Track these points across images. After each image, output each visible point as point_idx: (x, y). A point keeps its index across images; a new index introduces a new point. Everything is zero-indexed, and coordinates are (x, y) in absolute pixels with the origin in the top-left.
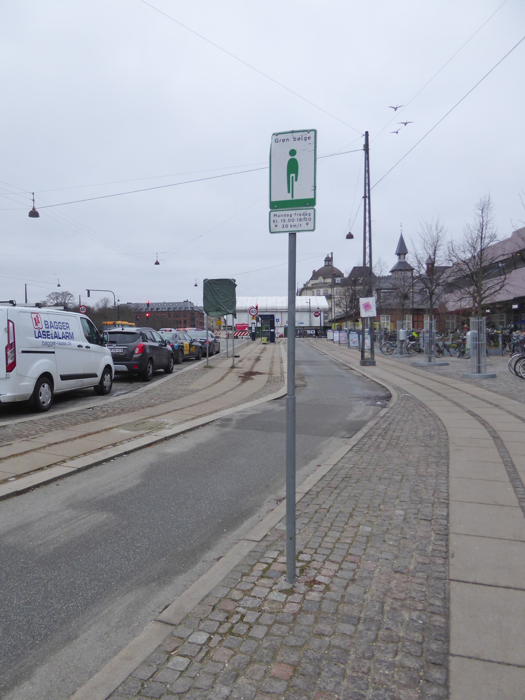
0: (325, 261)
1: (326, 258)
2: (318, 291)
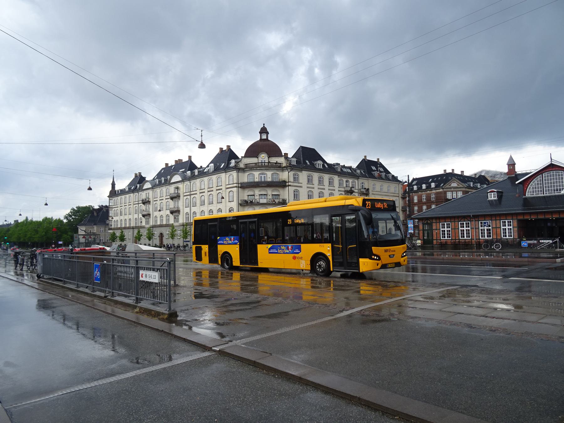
0: (261, 133)
1: (262, 129)
2: (263, 174)
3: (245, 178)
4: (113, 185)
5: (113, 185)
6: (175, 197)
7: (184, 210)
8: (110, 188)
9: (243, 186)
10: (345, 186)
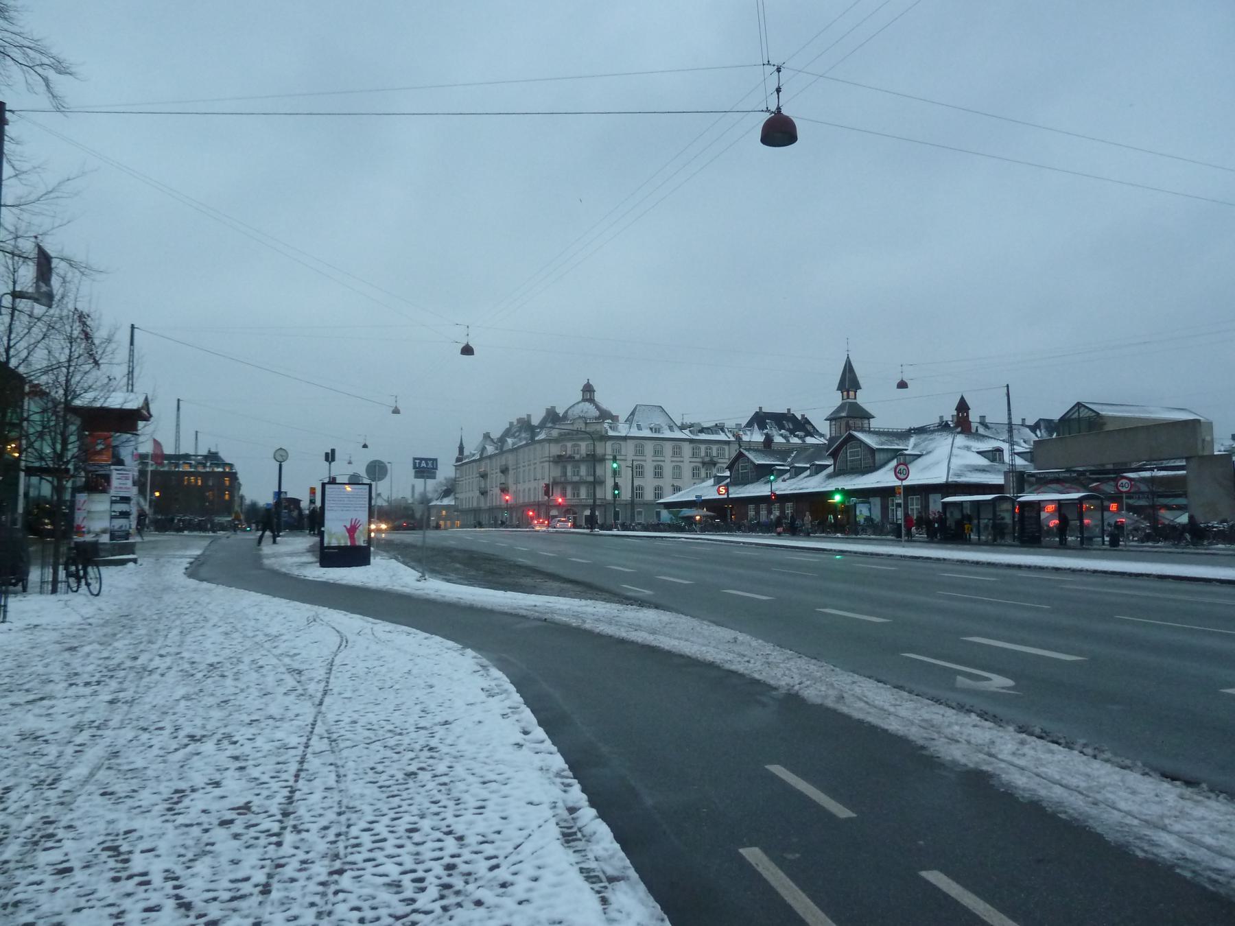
3: (555, 450)
4: (461, 449)
5: (461, 449)
6: (504, 471)
7: (512, 488)
8: (456, 454)
9: (559, 460)
10: (703, 454)
